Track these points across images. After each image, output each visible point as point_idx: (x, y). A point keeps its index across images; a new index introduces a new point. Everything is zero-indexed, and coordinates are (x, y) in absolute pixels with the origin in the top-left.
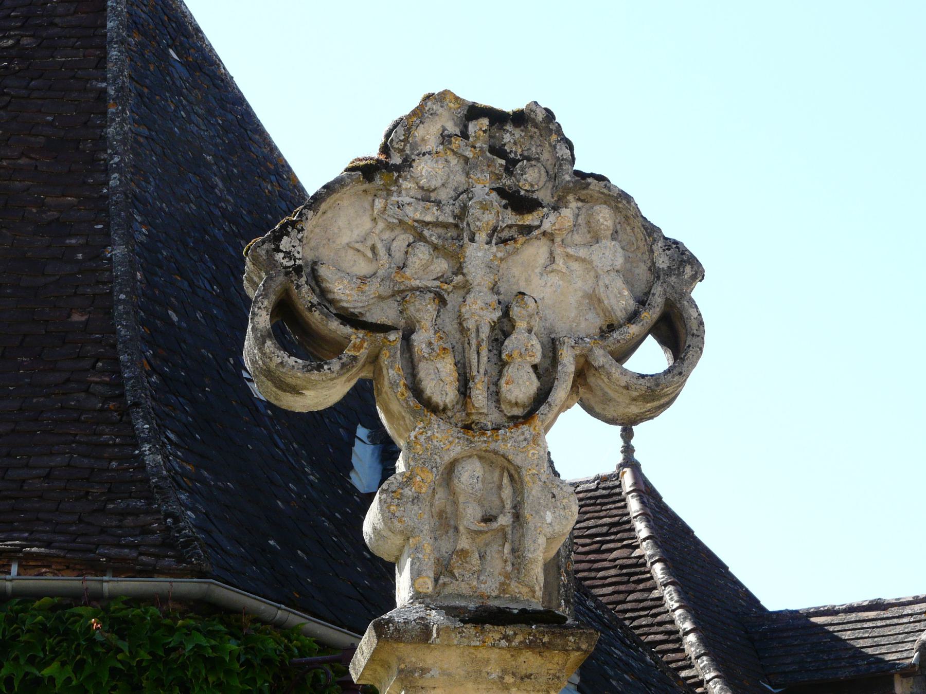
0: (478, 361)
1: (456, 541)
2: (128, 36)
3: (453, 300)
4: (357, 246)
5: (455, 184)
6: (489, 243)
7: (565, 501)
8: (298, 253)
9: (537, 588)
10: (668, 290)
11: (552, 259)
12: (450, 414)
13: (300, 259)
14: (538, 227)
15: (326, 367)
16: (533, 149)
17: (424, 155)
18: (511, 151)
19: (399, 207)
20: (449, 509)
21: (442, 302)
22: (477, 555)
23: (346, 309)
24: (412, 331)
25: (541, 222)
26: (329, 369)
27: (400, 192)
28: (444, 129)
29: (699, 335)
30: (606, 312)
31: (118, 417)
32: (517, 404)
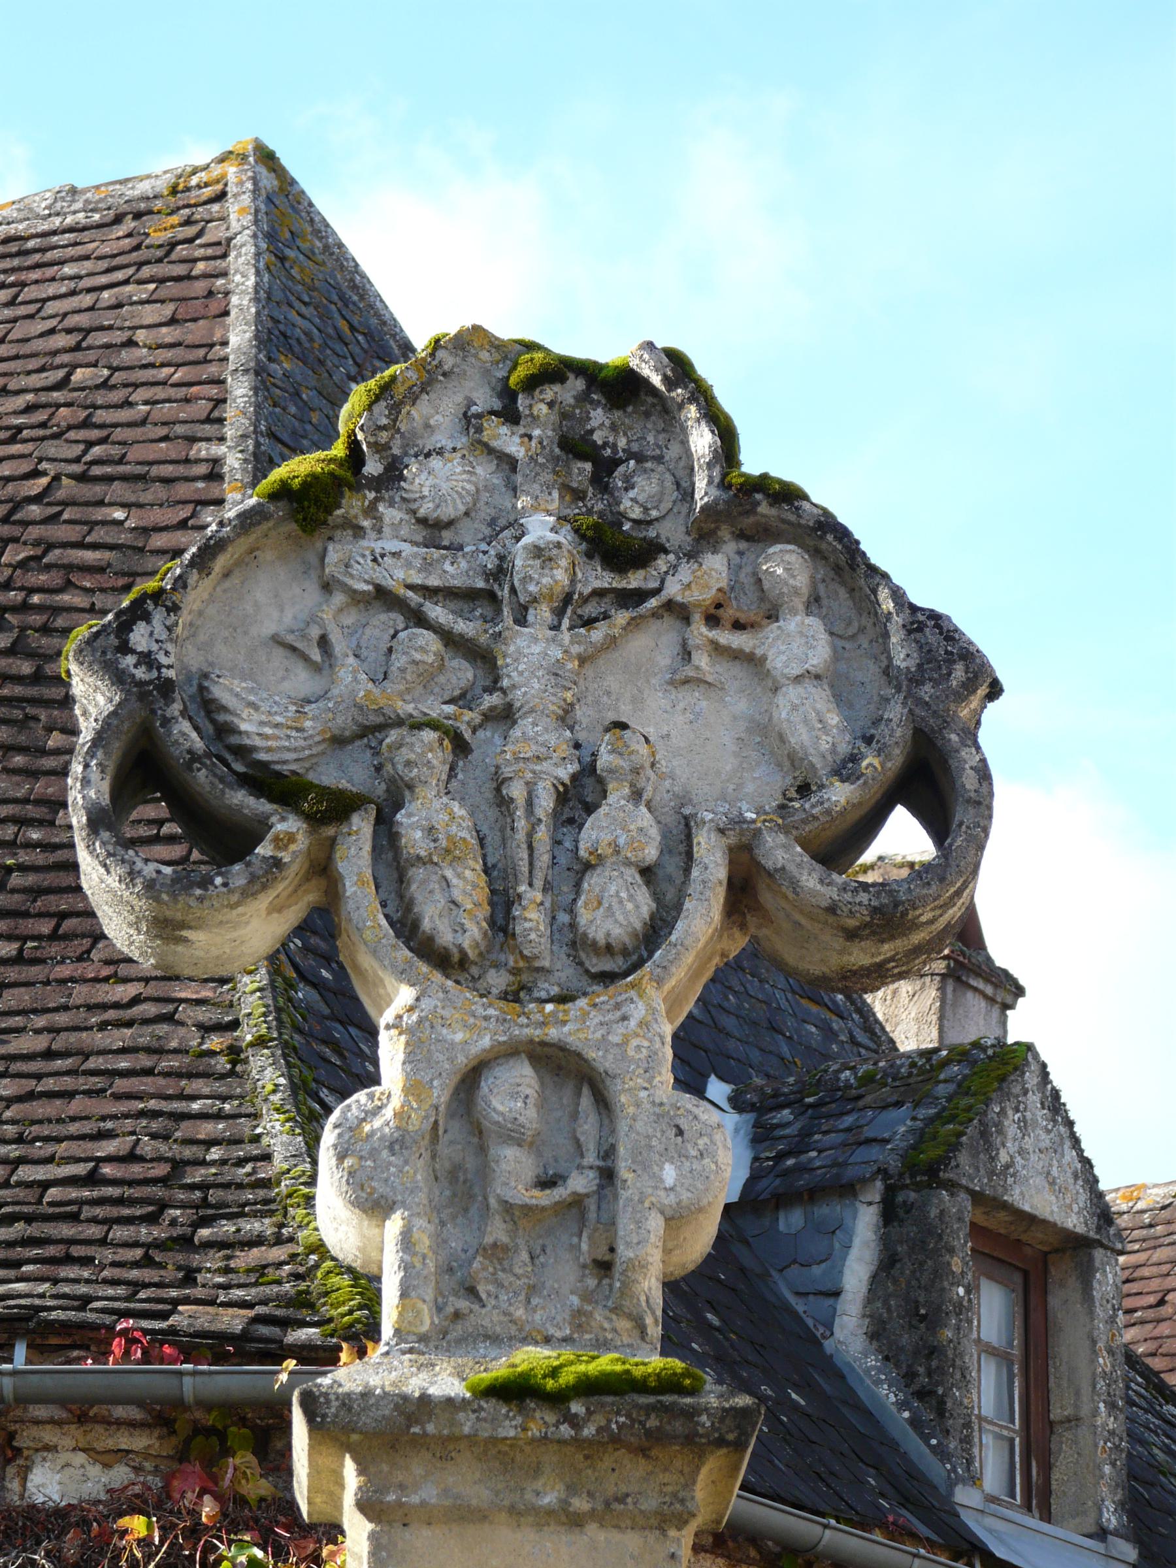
0: (531, 864)
1: (482, 1232)
2: (270, 359)
3: (485, 741)
4: (290, 639)
5: (492, 512)
6: (556, 628)
7: (701, 1142)
8: (167, 653)
9: (649, 1320)
10: (917, 711)
11: (686, 654)
12: (475, 971)
13: (169, 667)
14: (656, 592)
15: (218, 881)
16: (651, 439)
17: (428, 455)
18: (605, 444)
19: (375, 560)
20: (471, 1163)
21: (461, 747)
22: (524, 1256)
23: (264, 765)
24: (398, 806)
25: (663, 582)
26: (225, 885)
27: (380, 531)
28: (471, 403)
29: (983, 804)
30: (794, 760)
31: (229, 1066)
32: (609, 948)
